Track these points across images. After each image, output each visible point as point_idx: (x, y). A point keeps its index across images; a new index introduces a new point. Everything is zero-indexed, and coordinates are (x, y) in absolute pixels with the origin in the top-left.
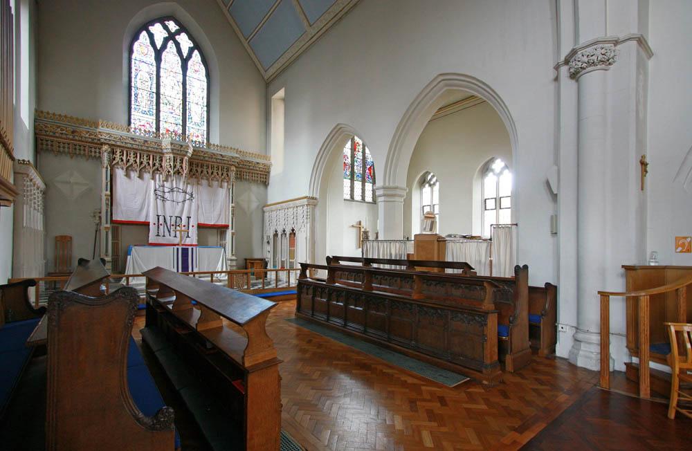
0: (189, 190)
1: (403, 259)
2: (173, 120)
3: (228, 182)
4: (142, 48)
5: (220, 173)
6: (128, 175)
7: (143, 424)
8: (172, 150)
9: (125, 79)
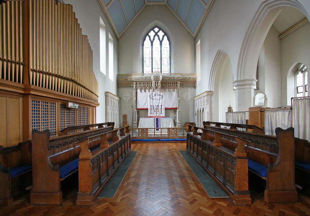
0: (161, 94)
1: (243, 124)
2: (157, 67)
3: (176, 89)
4: (147, 42)
5: (173, 85)
6: (141, 91)
7: (51, 167)
8: (154, 79)
9: (141, 56)
